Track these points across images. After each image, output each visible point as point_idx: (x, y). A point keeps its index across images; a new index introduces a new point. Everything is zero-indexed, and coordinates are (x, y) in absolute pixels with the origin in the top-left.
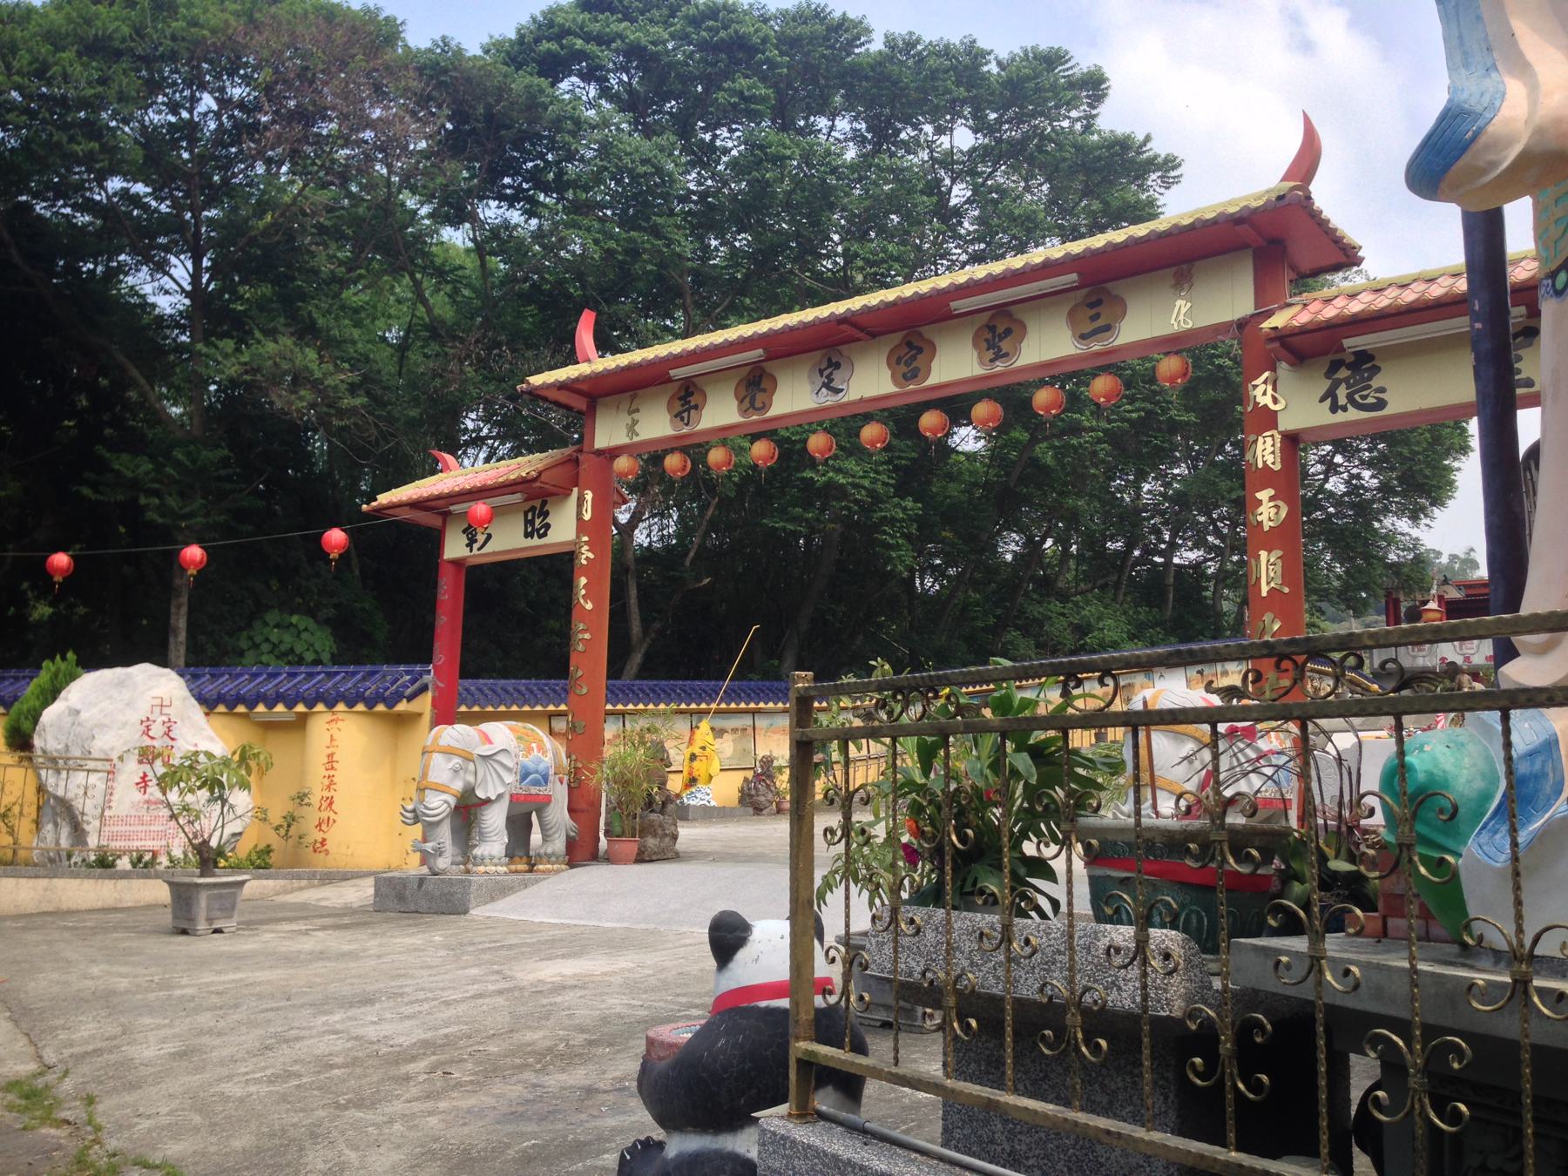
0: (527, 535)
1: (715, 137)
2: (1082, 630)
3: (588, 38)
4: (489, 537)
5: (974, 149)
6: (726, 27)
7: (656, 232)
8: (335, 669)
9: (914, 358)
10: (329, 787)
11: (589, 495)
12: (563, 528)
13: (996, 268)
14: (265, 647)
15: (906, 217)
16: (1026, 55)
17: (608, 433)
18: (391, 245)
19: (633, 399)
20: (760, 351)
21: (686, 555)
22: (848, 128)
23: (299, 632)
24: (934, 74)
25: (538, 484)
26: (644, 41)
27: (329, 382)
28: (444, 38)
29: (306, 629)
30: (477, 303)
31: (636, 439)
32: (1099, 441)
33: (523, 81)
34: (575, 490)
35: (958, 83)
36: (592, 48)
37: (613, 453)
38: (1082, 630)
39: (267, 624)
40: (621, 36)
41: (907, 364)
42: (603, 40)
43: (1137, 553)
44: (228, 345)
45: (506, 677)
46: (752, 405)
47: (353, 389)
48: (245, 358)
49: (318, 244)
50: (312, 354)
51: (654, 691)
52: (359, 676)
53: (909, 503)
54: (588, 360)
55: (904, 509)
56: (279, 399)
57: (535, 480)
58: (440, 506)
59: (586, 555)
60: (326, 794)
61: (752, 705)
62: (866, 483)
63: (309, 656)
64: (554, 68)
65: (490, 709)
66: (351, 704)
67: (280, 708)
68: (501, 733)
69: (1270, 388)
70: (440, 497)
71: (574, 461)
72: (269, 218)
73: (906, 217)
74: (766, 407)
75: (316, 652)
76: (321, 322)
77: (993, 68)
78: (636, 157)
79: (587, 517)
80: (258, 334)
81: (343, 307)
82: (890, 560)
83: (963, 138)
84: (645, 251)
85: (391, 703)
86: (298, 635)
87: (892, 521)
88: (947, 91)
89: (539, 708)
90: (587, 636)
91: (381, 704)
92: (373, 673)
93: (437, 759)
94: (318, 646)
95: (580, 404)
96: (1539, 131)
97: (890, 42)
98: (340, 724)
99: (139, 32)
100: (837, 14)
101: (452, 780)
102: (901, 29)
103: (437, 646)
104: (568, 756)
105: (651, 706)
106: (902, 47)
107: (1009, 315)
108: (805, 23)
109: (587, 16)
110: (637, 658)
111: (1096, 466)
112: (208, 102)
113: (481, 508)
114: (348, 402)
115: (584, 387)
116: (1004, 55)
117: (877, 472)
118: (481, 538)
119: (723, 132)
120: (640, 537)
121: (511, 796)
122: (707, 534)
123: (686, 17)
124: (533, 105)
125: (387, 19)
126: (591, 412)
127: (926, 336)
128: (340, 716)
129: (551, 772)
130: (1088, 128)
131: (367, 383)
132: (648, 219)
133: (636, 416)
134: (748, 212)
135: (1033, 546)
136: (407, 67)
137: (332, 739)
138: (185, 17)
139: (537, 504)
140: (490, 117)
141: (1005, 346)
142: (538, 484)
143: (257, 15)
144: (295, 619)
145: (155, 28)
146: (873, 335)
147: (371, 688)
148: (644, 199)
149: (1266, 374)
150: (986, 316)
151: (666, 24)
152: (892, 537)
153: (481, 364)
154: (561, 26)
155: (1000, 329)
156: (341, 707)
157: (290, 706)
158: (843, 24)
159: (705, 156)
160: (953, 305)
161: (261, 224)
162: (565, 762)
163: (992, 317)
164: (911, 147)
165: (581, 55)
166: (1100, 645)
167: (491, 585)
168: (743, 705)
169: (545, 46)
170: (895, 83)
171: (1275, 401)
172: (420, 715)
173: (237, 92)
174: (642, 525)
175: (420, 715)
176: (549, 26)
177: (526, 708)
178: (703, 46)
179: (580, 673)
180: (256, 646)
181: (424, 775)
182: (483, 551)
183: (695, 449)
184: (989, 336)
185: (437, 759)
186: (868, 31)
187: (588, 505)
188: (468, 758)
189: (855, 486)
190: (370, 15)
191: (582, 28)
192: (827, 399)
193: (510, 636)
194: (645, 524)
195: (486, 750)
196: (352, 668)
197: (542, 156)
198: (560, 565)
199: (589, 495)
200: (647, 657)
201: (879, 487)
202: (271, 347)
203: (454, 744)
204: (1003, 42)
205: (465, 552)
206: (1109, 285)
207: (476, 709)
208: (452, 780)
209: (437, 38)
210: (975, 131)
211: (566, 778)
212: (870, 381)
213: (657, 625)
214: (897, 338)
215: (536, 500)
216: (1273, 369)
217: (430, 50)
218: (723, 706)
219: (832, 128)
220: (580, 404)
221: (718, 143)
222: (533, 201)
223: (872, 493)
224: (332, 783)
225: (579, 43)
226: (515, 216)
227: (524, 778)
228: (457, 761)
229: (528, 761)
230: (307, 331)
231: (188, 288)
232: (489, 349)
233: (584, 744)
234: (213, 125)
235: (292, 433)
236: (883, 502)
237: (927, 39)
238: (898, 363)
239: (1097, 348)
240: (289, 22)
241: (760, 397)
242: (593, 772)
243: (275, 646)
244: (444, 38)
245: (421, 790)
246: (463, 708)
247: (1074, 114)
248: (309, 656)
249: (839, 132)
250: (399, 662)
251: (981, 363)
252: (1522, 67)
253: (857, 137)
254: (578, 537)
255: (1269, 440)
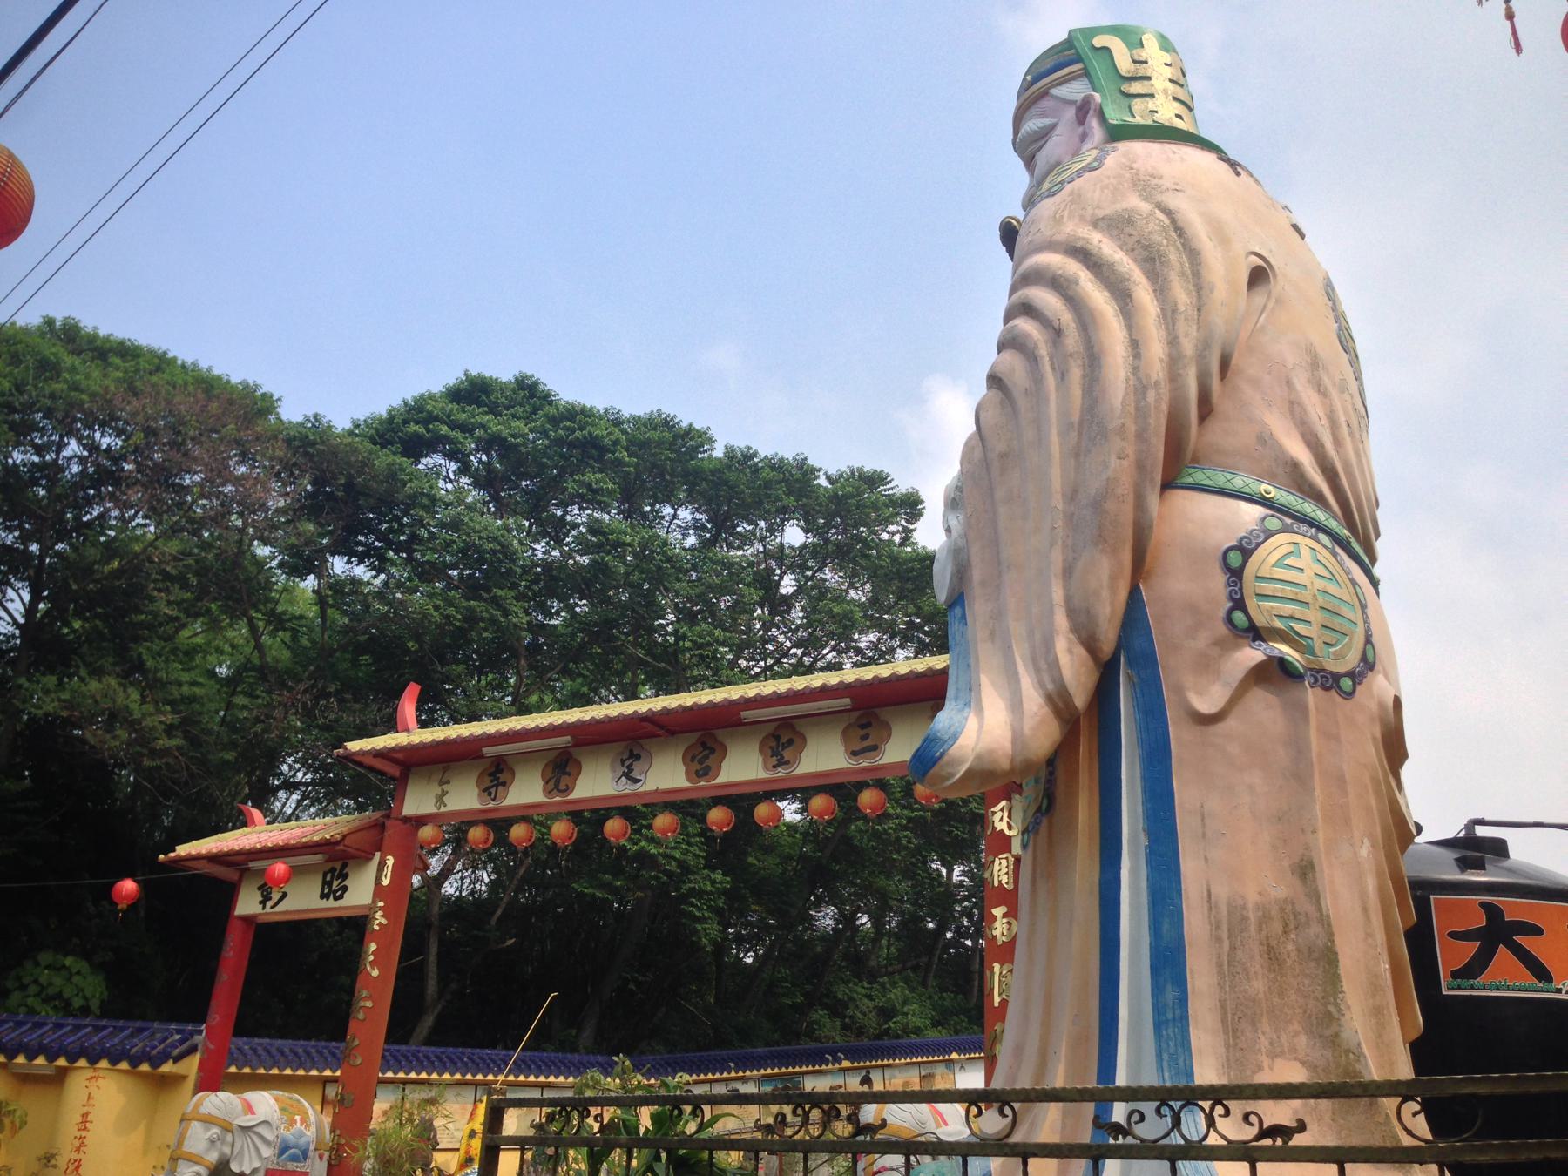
0: (324, 896)
1: (566, 513)
2: (887, 1013)
3: (453, 426)
4: (284, 895)
5: (804, 546)
6: (581, 429)
7: (496, 602)
8: (104, 1022)
9: (706, 757)
10: (78, 1149)
11: (390, 861)
12: (360, 892)
13: (782, 686)
14: (33, 989)
15: (728, 615)
16: (852, 471)
17: (417, 801)
18: (233, 588)
19: (445, 770)
20: (568, 738)
21: (493, 913)
22: (689, 517)
23: (71, 975)
24: (767, 485)
25: (341, 847)
26: (505, 433)
27: (148, 722)
28: (316, 416)
29: (78, 973)
30: (312, 654)
31: (443, 809)
32: (905, 828)
33: (385, 459)
34: (378, 854)
35: (789, 493)
36: (456, 434)
37: (420, 821)
38: (887, 1013)
39: (37, 964)
40: (483, 426)
41: (700, 762)
42: (466, 429)
43: (949, 935)
44: (51, 681)
45: (282, 1037)
46: (557, 787)
47: (170, 730)
48: (65, 696)
49: (160, 590)
50: (135, 695)
51: (440, 1060)
52: (127, 1032)
53: (718, 876)
54: (407, 730)
55: (713, 882)
56: (91, 734)
57: (338, 843)
58: (240, 862)
59: (379, 919)
60: (75, 1156)
61: (542, 1079)
62: (677, 854)
63: (77, 1002)
64: (416, 448)
65: (262, 1071)
66: (114, 1062)
67: (40, 1060)
68: (265, 1102)
69: (1006, 814)
70: (241, 853)
71: (379, 826)
72: (116, 564)
73: (728, 615)
74: (569, 789)
75: (85, 998)
76: (150, 663)
77: (823, 481)
78: (484, 534)
79: (386, 882)
80: (83, 672)
81: (174, 651)
82: (696, 931)
83: (794, 535)
84: (482, 620)
85: (156, 1064)
86: (69, 979)
87: (700, 893)
88: (778, 499)
89: (314, 1073)
90: (369, 1004)
91: (147, 1064)
92: (141, 1030)
93: (196, 1127)
94: (88, 993)
95: (394, 770)
96: (979, 757)
97: (729, 451)
98: (100, 1082)
99: (19, 388)
100: (684, 424)
101: (208, 1150)
102: (740, 443)
103: (214, 1004)
104: (333, 1131)
105: (435, 1076)
106: (741, 460)
107: (792, 727)
108: (655, 429)
109: (455, 406)
110: (428, 1021)
111: (898, 852)
112: (73, 448)
113: (280, 868)
114: (163, 742)
115: (400, 756)
116: (833, 471)
117: (689, 844)
118: (276, 896)
119: (575, 509)
120: (449, 889)
121: (267, 1171)
122: (519, 890)
123: (546, 415)
124: (392, 475)
125: (264, 395)
126: (402, 782)
127: (720, 738)
128: (101, 1073)
129: (312, 1147)
130: (905, 541)
131: (187, 726)
132: (489, 591)
133: (446, 787)
134: (591, 582)
135: (847, 920)
136: (275, 438)
137: (89, 1097)
138: (66, 381)
139: (338, 865)
140: (349, 486)
141: (787, 754)
142: (341, 847)
143: (138, 384)
144: (68, 961)
145: (36, 386)
146: (673, 733)
147: (138, 1046)
148: (489, 570)
149: (1004, 803)
150: (771, 727)
151: (527, 419)
152: (699, 909)
153: (308, 713)
154: (430, 413)
155: (784, 740)
156: (104, 1064)
157: (52, 1058)
158: (690, 432)
159: (556, 531)
160: (743, 714)
161: (106, 569)
162: (328, 1136)
163: (777, 728)
164: (746, 539)
165: (445, 439)
166: (903, 1030)
167: (281, 942)
168: (532, 1078)
169: (413, 428)
170: (731, 488)
171: (1010, 827)
172: (184, 1077)
173: (105, 442)
174: (452, 878)
175: (184, 1077)
176: (418, 410)
177: (301, 1072)
178: (560, 442)
179: (356, 1042)
180: (23, 988)
181: (180, 1143)
182: (276, 909)
183: (499, 825)
184: (774, 744)
185: (196, 1127)
186: (711, 441)
187: (388, 871)
188: (227, 1128)
189: (666, 856)
190: (248, 391)
191: (449, 416)
192: (626, 787)
193: (292, 997)
194: (458, 876)
195: (247, 1121)
196: (121, 1023)
197: (398, 519)
198: (356, 925)
199: (390, 861)
200: (440, 1019)
201: (689, 858)
202: (94, 685)
203: (215, 1112)
204: (831, 459)
205: (258, 909)
206: (877, 710)
207: (247, 1070)
208: (208, 1150)
209: (310, 414)
210: (806, 531)
211: (326, 1155)
212: (666, 774)
213: (454, 986)
214: (693, 737)
215: (335, 861)
216: (1009, 800)
217: (301, 424)
218: (511, 1078)
219: (674, 516)
220: (394, 770)
221: (569, 518)
222: (383, 559)
223: (681, 863)
224: (82, 1145)
225: (444, 429)
226: (361, 571)
227: (282, 1152)
228: (215, 1131)
229: (288, 1134)
230: (132, 669)
231: (22, 621)
232: (316, 699)
233: (350, 1117)
234: (75, 469)
235: (100, 770)
236: (694, 873)
237: (763, 453)
238: (692, 760)
239: (865, 764)
240: (168, 393)
241: (565, 780)
242: (355, 1150)
243: (43, 988)
244: (316, 416)
245: (174, 1160)
246: (233, 1069)
247: (892, 528)
248: (77, 1002)
249: (680, 526)
250: (170, 1020)
251: (766, 768)
252: (980, 711)
253: (698, 527)
254: (374, 901)
255: (1004, 862)
